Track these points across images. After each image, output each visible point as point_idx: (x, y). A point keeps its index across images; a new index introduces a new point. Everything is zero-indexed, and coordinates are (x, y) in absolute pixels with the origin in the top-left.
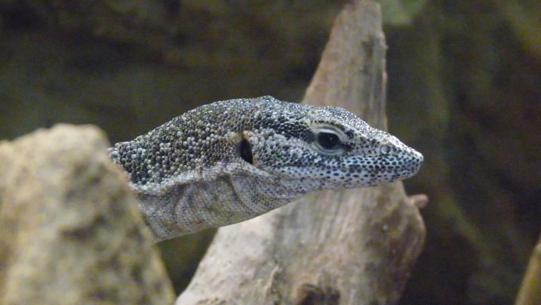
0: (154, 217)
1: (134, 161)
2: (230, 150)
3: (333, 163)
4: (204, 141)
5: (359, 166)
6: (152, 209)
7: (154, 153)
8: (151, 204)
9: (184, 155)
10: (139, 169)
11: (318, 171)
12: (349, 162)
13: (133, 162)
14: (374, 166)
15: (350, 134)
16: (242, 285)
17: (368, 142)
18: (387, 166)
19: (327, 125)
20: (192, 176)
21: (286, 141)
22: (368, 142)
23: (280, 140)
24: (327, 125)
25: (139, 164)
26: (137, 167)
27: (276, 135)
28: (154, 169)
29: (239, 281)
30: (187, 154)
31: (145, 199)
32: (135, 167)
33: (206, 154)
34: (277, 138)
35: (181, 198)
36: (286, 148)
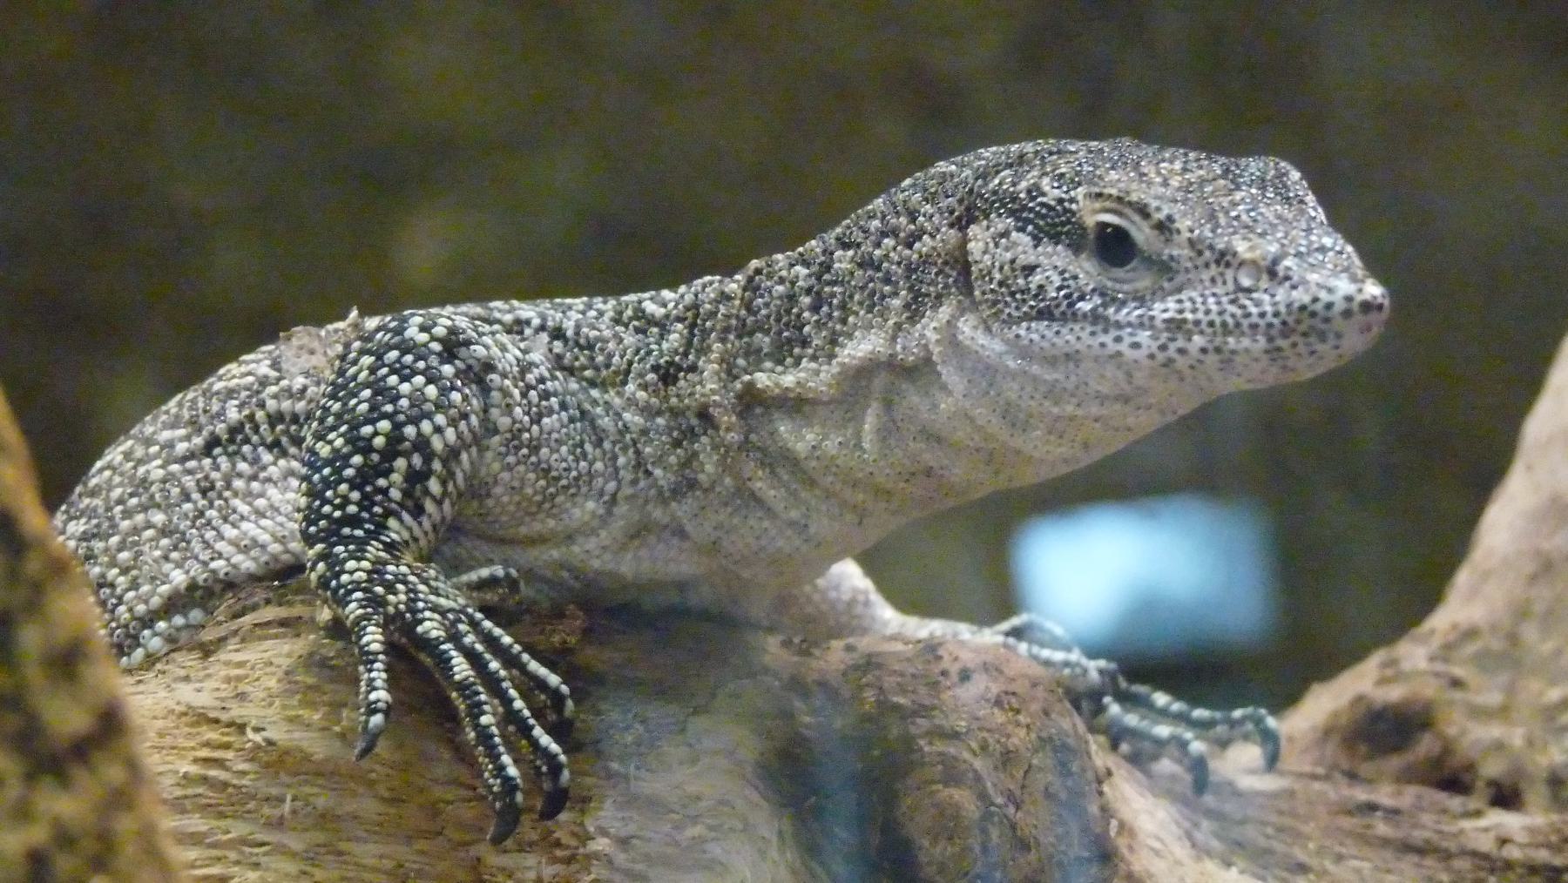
0: (818, 458)
1: (778, 302)
2: (949, 276)
3: (1130, 313)
4: (908, 252)
5: (1185, 321)
6: (810, 437)
7: (819, 279)
8: (810, 425)
9: (871, 285)
10: (787, 325)
11: (1093, 334)
12: (1165, 309)
13: (775, 305)
14: (1218, 320)
15: (1164, 228)
16: (1534, 579)
17: (1207, 254)
18: (1245, 323)
19: (1108, 204)
20: (870, 347)
21: (1031, 251)
22: (1207, 254)
23: (1020, 249)
24: (1108, 204)
25: (788, 312)
26: (785, 320)
27: (1014, 234)
28: (817, 322)
29: (1530, 568)
30: (879, 285)
31: (798, 411)
32: (778, 320)
33: (910, 289)
34: (1015, 244)
35: (870, 406)
36: (1030, 270)
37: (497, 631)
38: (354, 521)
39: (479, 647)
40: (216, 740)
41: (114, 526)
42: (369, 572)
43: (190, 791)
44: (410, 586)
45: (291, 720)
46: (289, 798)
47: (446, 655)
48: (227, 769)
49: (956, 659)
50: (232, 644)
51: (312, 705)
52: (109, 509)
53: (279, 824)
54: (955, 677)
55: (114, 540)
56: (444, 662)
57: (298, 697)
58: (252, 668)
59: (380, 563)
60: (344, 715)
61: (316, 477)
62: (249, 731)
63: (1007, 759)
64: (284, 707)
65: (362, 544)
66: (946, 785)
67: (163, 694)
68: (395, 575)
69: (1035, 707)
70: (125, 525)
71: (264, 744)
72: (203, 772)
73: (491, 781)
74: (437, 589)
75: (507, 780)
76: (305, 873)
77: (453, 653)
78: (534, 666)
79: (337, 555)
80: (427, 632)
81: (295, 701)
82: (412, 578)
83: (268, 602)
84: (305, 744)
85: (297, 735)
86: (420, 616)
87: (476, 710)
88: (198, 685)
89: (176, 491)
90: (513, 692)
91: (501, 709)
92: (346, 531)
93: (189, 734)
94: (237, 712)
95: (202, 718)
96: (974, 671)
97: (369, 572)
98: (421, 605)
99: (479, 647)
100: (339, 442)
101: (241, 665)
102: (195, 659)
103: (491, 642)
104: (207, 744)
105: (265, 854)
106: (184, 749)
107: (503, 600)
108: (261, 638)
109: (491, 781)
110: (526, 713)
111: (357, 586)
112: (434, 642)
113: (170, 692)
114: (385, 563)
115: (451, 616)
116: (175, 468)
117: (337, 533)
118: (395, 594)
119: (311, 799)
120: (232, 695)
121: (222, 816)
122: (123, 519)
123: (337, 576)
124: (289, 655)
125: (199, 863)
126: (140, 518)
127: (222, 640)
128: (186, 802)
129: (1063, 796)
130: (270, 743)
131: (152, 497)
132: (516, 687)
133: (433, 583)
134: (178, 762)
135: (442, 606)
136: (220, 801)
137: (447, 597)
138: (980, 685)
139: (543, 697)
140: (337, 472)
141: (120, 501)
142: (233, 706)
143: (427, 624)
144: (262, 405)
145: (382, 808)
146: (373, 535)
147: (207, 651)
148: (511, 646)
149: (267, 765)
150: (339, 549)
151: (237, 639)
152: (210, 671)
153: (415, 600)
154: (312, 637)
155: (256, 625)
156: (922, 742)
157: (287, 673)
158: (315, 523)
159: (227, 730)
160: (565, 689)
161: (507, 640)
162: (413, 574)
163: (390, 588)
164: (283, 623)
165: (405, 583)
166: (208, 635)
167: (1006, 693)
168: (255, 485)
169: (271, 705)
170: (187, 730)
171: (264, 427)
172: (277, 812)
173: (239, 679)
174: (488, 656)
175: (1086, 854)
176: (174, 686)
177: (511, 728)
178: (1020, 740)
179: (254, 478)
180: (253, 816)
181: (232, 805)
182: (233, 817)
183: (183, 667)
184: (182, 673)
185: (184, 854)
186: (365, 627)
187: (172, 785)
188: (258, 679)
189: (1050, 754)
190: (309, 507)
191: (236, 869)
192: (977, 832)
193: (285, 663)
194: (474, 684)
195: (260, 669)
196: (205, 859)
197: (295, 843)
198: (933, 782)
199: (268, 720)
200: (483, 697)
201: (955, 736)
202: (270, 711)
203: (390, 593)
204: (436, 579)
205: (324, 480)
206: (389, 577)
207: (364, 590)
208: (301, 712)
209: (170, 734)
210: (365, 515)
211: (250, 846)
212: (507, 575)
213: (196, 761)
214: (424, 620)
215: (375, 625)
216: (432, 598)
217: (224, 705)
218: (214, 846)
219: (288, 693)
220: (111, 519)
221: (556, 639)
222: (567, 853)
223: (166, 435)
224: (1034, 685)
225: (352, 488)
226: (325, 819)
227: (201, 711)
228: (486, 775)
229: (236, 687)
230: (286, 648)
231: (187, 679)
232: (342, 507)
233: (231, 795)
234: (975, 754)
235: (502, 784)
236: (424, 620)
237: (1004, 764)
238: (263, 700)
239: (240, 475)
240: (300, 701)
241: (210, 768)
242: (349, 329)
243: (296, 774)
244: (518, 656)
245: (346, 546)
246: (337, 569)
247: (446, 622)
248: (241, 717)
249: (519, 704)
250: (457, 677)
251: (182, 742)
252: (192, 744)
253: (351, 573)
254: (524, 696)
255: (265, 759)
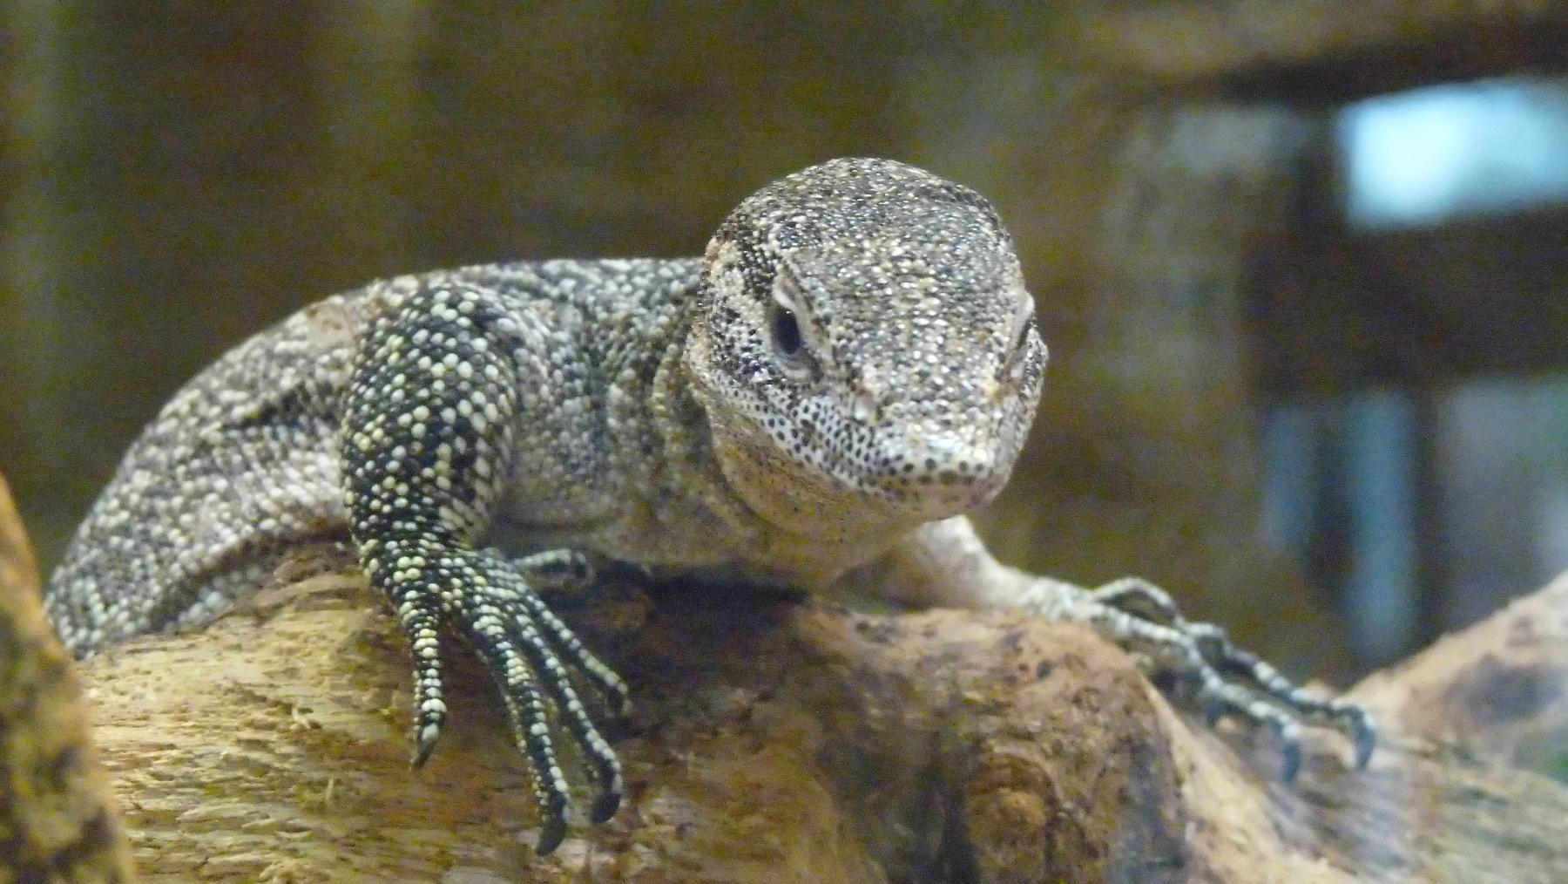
37: (557, 624)
38: (406, 514)
39: (538, 642)
40: (262, 720)
41: (177, 486)
42: (422, 569)
43: (230, 774)
44: (467, 579)
45: (340, 701)
46: (331, 783)
47: (503, 655)
48: (271, 751)
49: (1038, 651)
50: (288, 612)
51: (364, 686)
52: (171, 467)
53: (319, 810)
54: (1033, 672)
55: (177, 501)
56: (501, 660)
57: (348, 676)
58: (306, 641)
59: (432, 558)
60: (394, 698)
61: (360, 472)
62: (295, 711)
63: (1080, 762)
64: (333, 687)
65: (414, 537)
66: (1014, 788)
67: (212, 662)
68: (450, 568)
69: (1116, 705)
70: (188, 486)
71: (308, 727)
72: (244, 754)
73: (539, 793)
74: (495, 578)
75: (554, 794)
76: (343, 860)
77: (510, 653)
78: (592, 663)
79: (389, 551)
80: (484, 629)
81: (344, 681)
82: (469, 571)
83: (327, 569)
84: (351, 729)
85: (345, 717)
86: (479, 611)
87: (528, 717)
88: (249, 655)
89: (237, 458)
90: (569, 692)
91: (555, 709)
92: (398, 525)
93: (235, 712)
94: (284, 691)
95: (246, 696)
96: (1056, 665)
97: (422, 569)
98: (478, 599)
99: (538, 642)
100: (378, 433)
101: (294, 636)
102: (247, 626)
103: (550, 634)
104: (251, 725)
105: (304, 840)
106: (227, 729)
107: (567, 584)
108: (318, 608)
109: (539, 793)
110: (582, 715)
111: (411, 584)
112: (491, 640)
113: (221, 660)
114: (439, 556)
115: (510, 608)
116: (234, 434)
117: (388, 528)
118: (450, 589)
119: (355, 784)
120: (283, 669)
121: (262, 799)
122: (187, 479)
123: (390, 573)
124: (343, 629)
125: (236, 848)
126: (202, 481)
127: (277, 608)
128: (226, 785)
129: (1138, 800)
130: (316, 726)
131: (213, 462)
132: (573, 686)
133: (491, 573)
134: (220, 743)
135: (500, 598)
136: (260, 785)
137: (506, 587)
138: (1061, 680)
139: (599, 695)
140: (381, 464)
141: (183, 461)
142: (282, 683)
143: (485, 620)
144: (311, 375)
145: (427, 794)
146: (423, 528)
147: (261, 617)
148: (569, 641)
149: (312, 748)
150: (392, 544)
151: (293, 607)
152: (263, 641)
153: (471, 595)
154: (369, 611)
155: (313, 594)
156: (992, 742)
157: (339, 651)
158: (365, 518)
159: (274, 709)
160: (623, 688)
161: (566, 634)
162: (470, 565)
163: (445, 584)
164: (341, 594)
165: (461, 576)
166: (264, 600)
167: (1087, 690)
168: (310, 456)
169: (320, 683)
170: (232, 707)
171: (315, 398)
172: (318, 797)
173: (291, 651)
174: (546, 652)
175: (1158, 860)
176: (225, 654)
177: (565, 729)
178: (1097, 741)
179: (310, 448)
180: (295, 800)
181: (273, 790)
182: (272, 801)
183: (236, 634)
184: (234, 640)
185: (220, 839)
186: (418, 630)
187: (213, 768)
188: (310, 654)
189: (1128, 755)
190: (357, 502)
191: (272, 855)
192: (1043, 838)
193: (341, 638)
194: (528, 689)
195: (314, 643)
196: (241, 845)
197: (335, 829)
198: (1003, 785)
199: (316, 700)
200: (536, 704)
201: (1028, 737)
202: (318, 691)
203: (447, 590)
204: (495, 567)
205: (367, 474)
206: (444, 572)
207: (419, 589)
208: (350, 693)
209: (213, 712)
210: (415, 507)
211: (287, 831)
212: (574, 560)
213: (239, 742)
214: (482, 615)
215: (428, 628)
216: (490, 590)
217: (272, 682)
218: (250, 831)
219: (338, 671)
220: (174, 478)
221: (618, 623)
222: (617, 840)
223: (227, 396)
224: (1117, 680)
225: (398, 482)
226: (368, 805)
227: (248, 688)
228: (535, 786)
229: (287, 661)
230: (341, 621)
231: (238, 647)
232: (390, 501)
233: (272, 779)
234: (1047, 757)
235: (550, 799)
236: (482, 615)
237: (1078, 768)
238: (313, 678)
239: (296, 446)
240: (350, 680)
241: (234, 776)
242: (373, 304)
243: (342, 758)
244: (576, 652)
245: (398, 540)
246: (390, 565)
247: (505, 615)
248: (288, 696)
249: (574, 705)
250: (512, 681)
251: (224, 721)
252: (236, 724)
253: (404, 570)
254: (581, 696)
255: (310, 741)
